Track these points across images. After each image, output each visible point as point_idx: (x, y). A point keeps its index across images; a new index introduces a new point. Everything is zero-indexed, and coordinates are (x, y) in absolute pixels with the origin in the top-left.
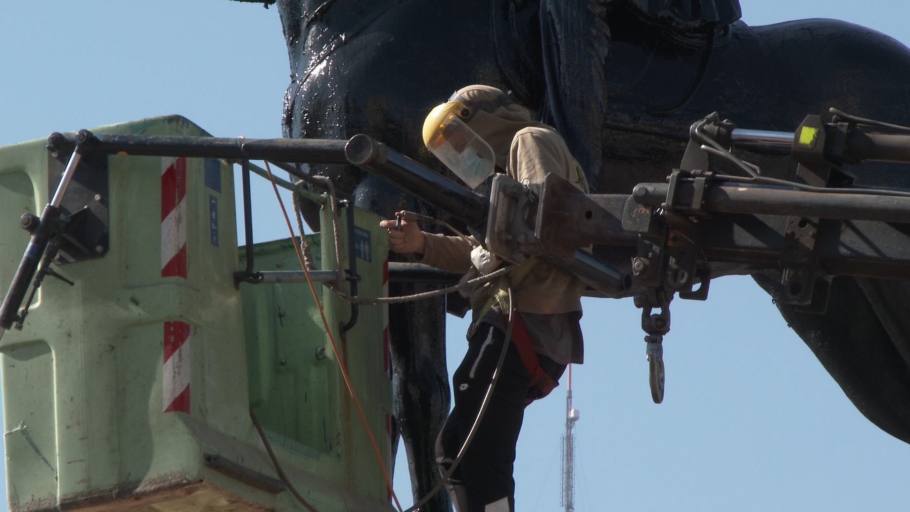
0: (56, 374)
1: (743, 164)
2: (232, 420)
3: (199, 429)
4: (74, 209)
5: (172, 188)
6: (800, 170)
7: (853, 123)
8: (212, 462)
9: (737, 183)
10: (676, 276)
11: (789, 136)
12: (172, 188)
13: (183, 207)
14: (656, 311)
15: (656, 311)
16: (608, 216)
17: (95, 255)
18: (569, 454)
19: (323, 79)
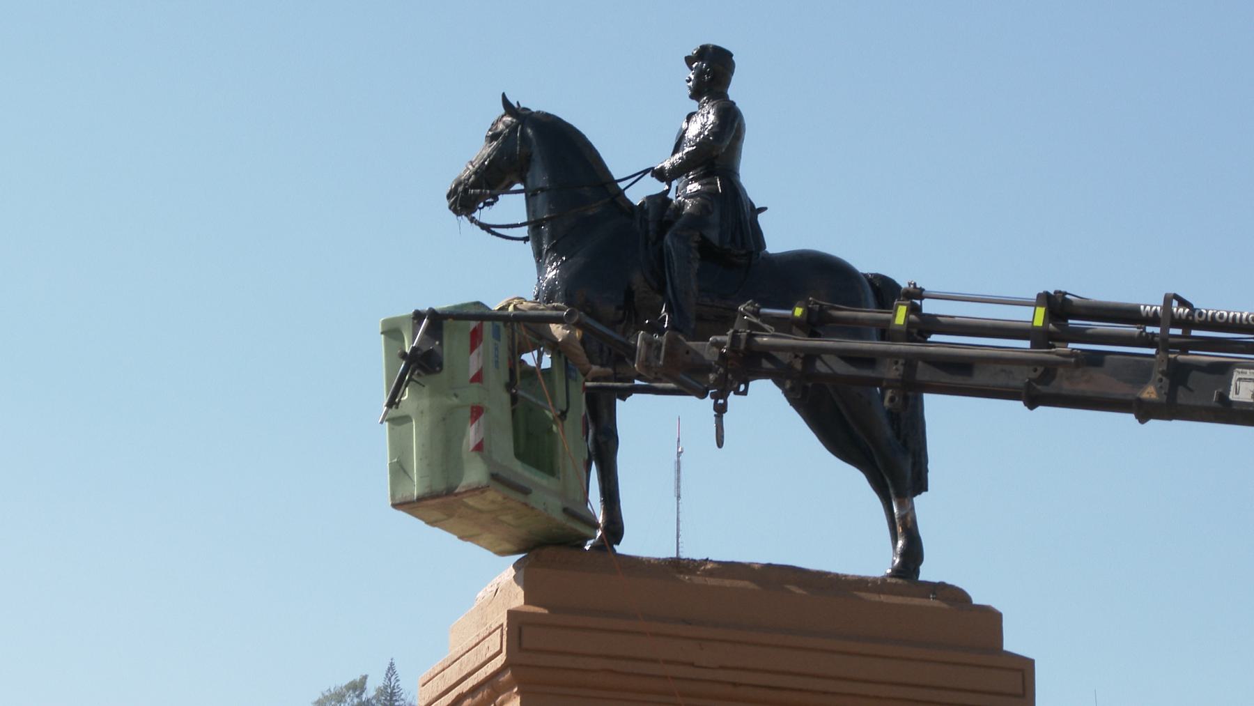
0: (415, 433)
1: (766, 326)
2: (504, 446)
3: (488, 460)
4: (425, 349)
5: (476, 337)
6: (794, 329)
7: (821, 306)
8: (495, 477)
9: (763, 336)
10: (731, 383)
11: (789, 312)
12: (476, 337)
13: (481, 348)
14: (721, 401)
15: (721, 401)
16: (696, 353)
17: (435, 372)
18: (678, 471)
19: (555, 280)
